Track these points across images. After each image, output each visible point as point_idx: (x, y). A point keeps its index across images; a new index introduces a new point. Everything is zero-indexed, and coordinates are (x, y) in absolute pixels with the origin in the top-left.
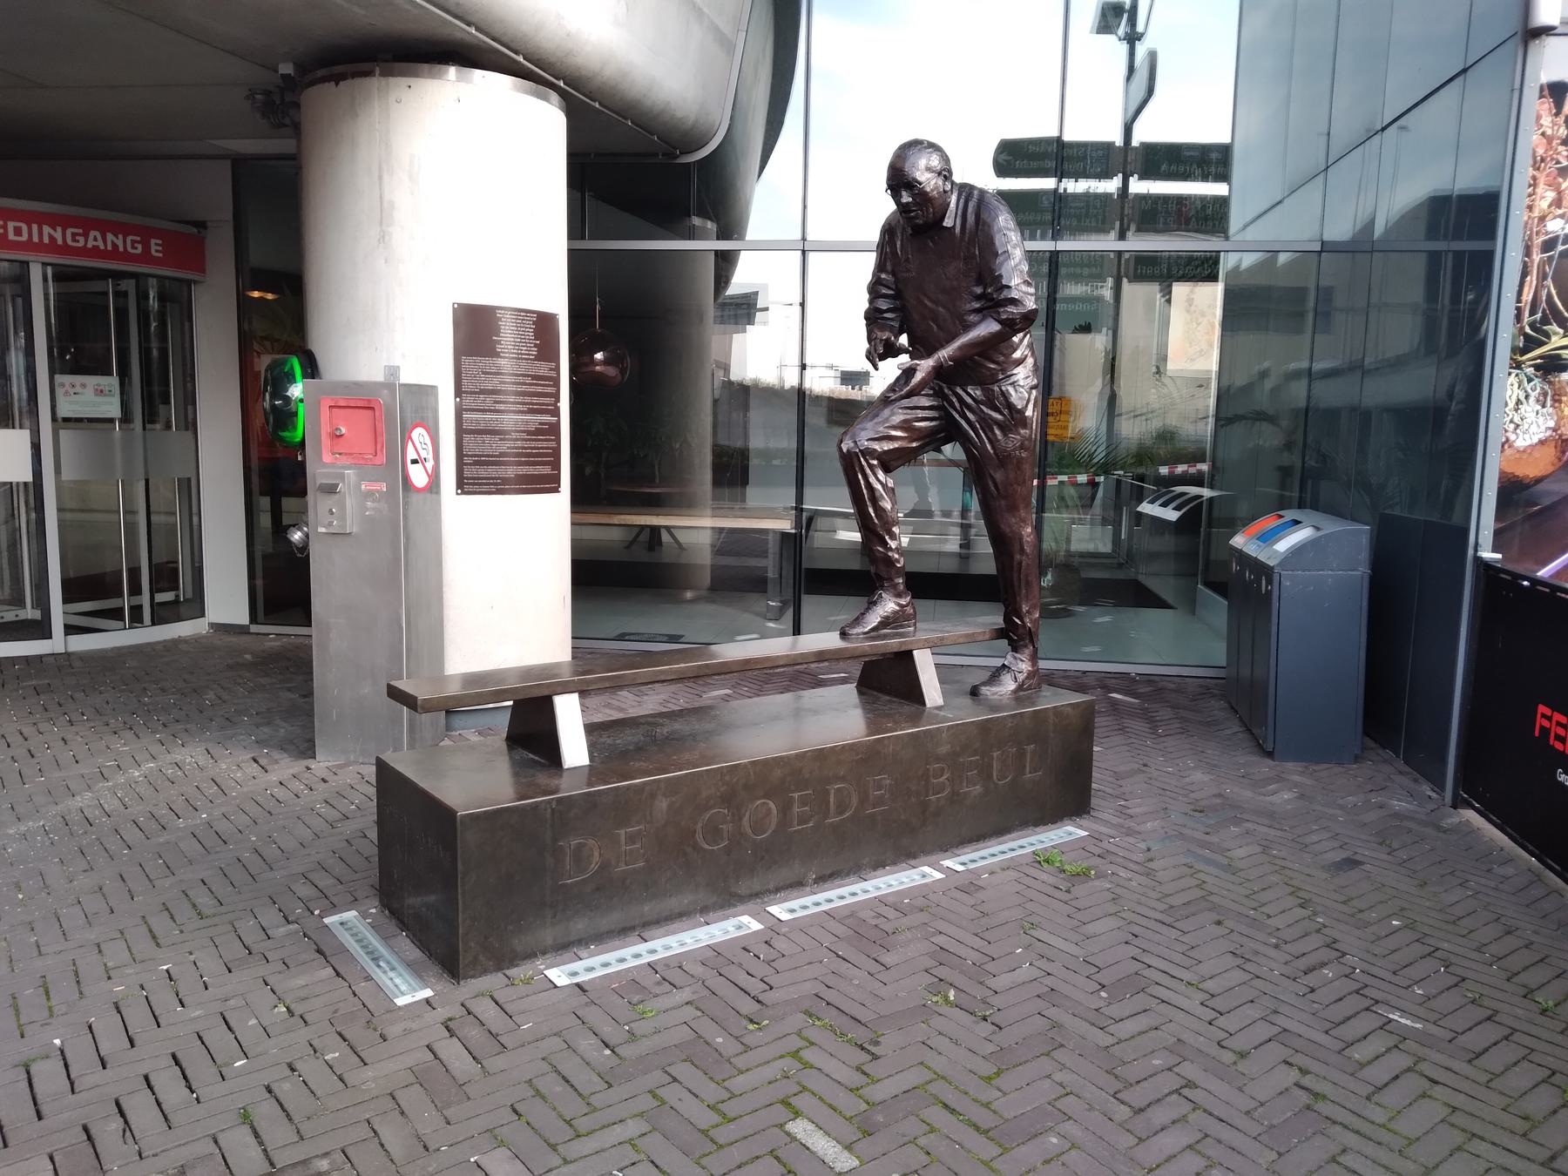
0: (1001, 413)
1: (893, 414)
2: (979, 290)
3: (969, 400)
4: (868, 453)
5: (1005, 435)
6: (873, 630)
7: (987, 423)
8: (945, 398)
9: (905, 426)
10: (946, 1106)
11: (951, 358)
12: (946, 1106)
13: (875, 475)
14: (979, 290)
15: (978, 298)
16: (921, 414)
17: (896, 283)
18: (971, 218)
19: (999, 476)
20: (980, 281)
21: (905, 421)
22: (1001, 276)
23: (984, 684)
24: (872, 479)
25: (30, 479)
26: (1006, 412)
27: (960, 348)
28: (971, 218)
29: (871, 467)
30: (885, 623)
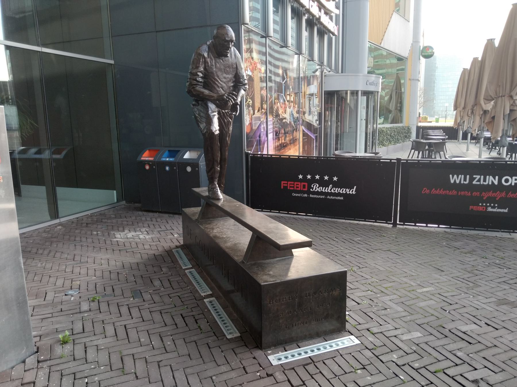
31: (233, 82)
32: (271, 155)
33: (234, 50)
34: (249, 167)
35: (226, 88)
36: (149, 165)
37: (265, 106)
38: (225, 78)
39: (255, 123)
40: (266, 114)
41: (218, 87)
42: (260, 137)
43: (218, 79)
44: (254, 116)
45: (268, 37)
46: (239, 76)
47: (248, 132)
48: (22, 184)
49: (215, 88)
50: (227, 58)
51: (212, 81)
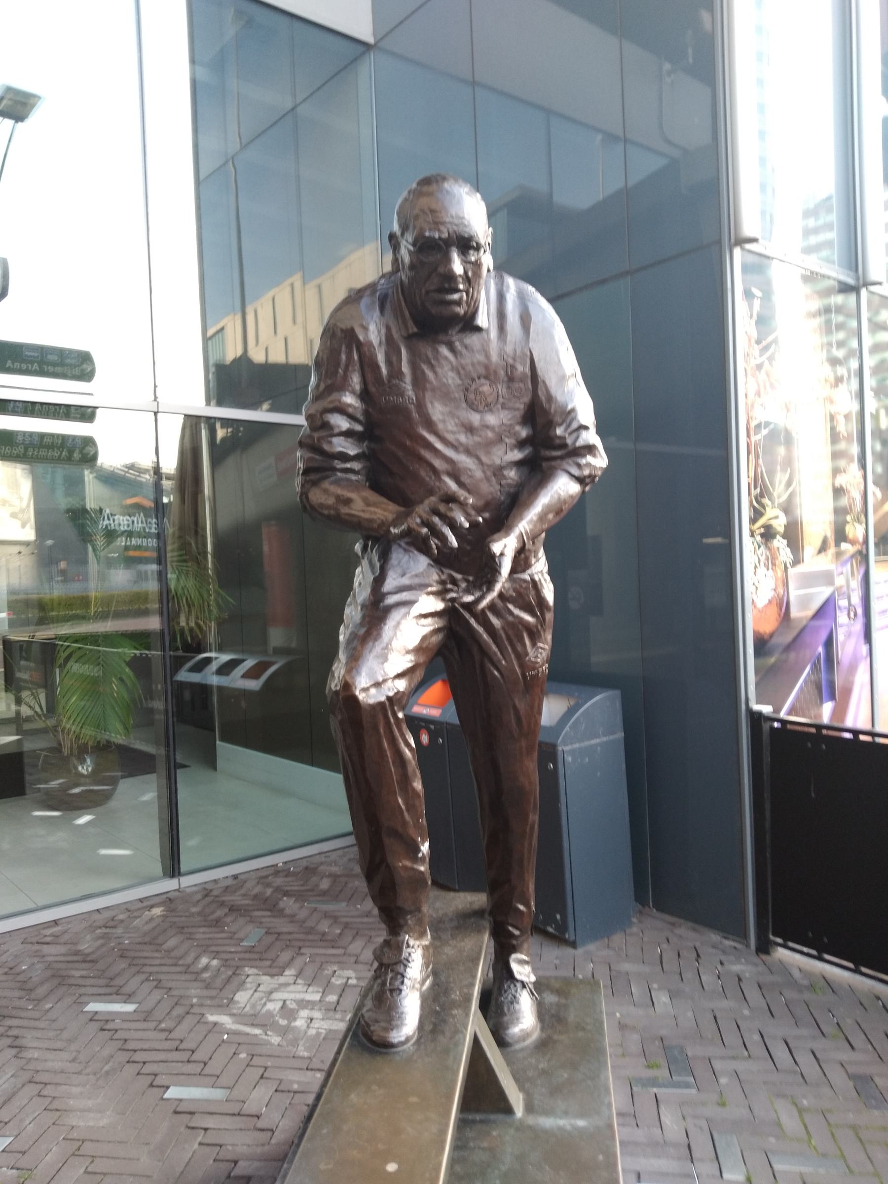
0: (533, 614)
17: (366, 413)
31: (521, 444)
32: (856, 733)
33: (522, 297)
34: (766, 769)
35: (479, 474)
36: (431, 734)
37: (855, 531)
38: (470, 429)
39: (805, 601)
40: (863, 557)
41: (435, 471)
42: (829, 643)
43: (432, 438)
44: (800, 569)
45: (866, 284)
46: (546, 412)
47: (767, 628)
48: (223, 739)
49: (416, 477)
50: (473, 340)
51: (402, 446)
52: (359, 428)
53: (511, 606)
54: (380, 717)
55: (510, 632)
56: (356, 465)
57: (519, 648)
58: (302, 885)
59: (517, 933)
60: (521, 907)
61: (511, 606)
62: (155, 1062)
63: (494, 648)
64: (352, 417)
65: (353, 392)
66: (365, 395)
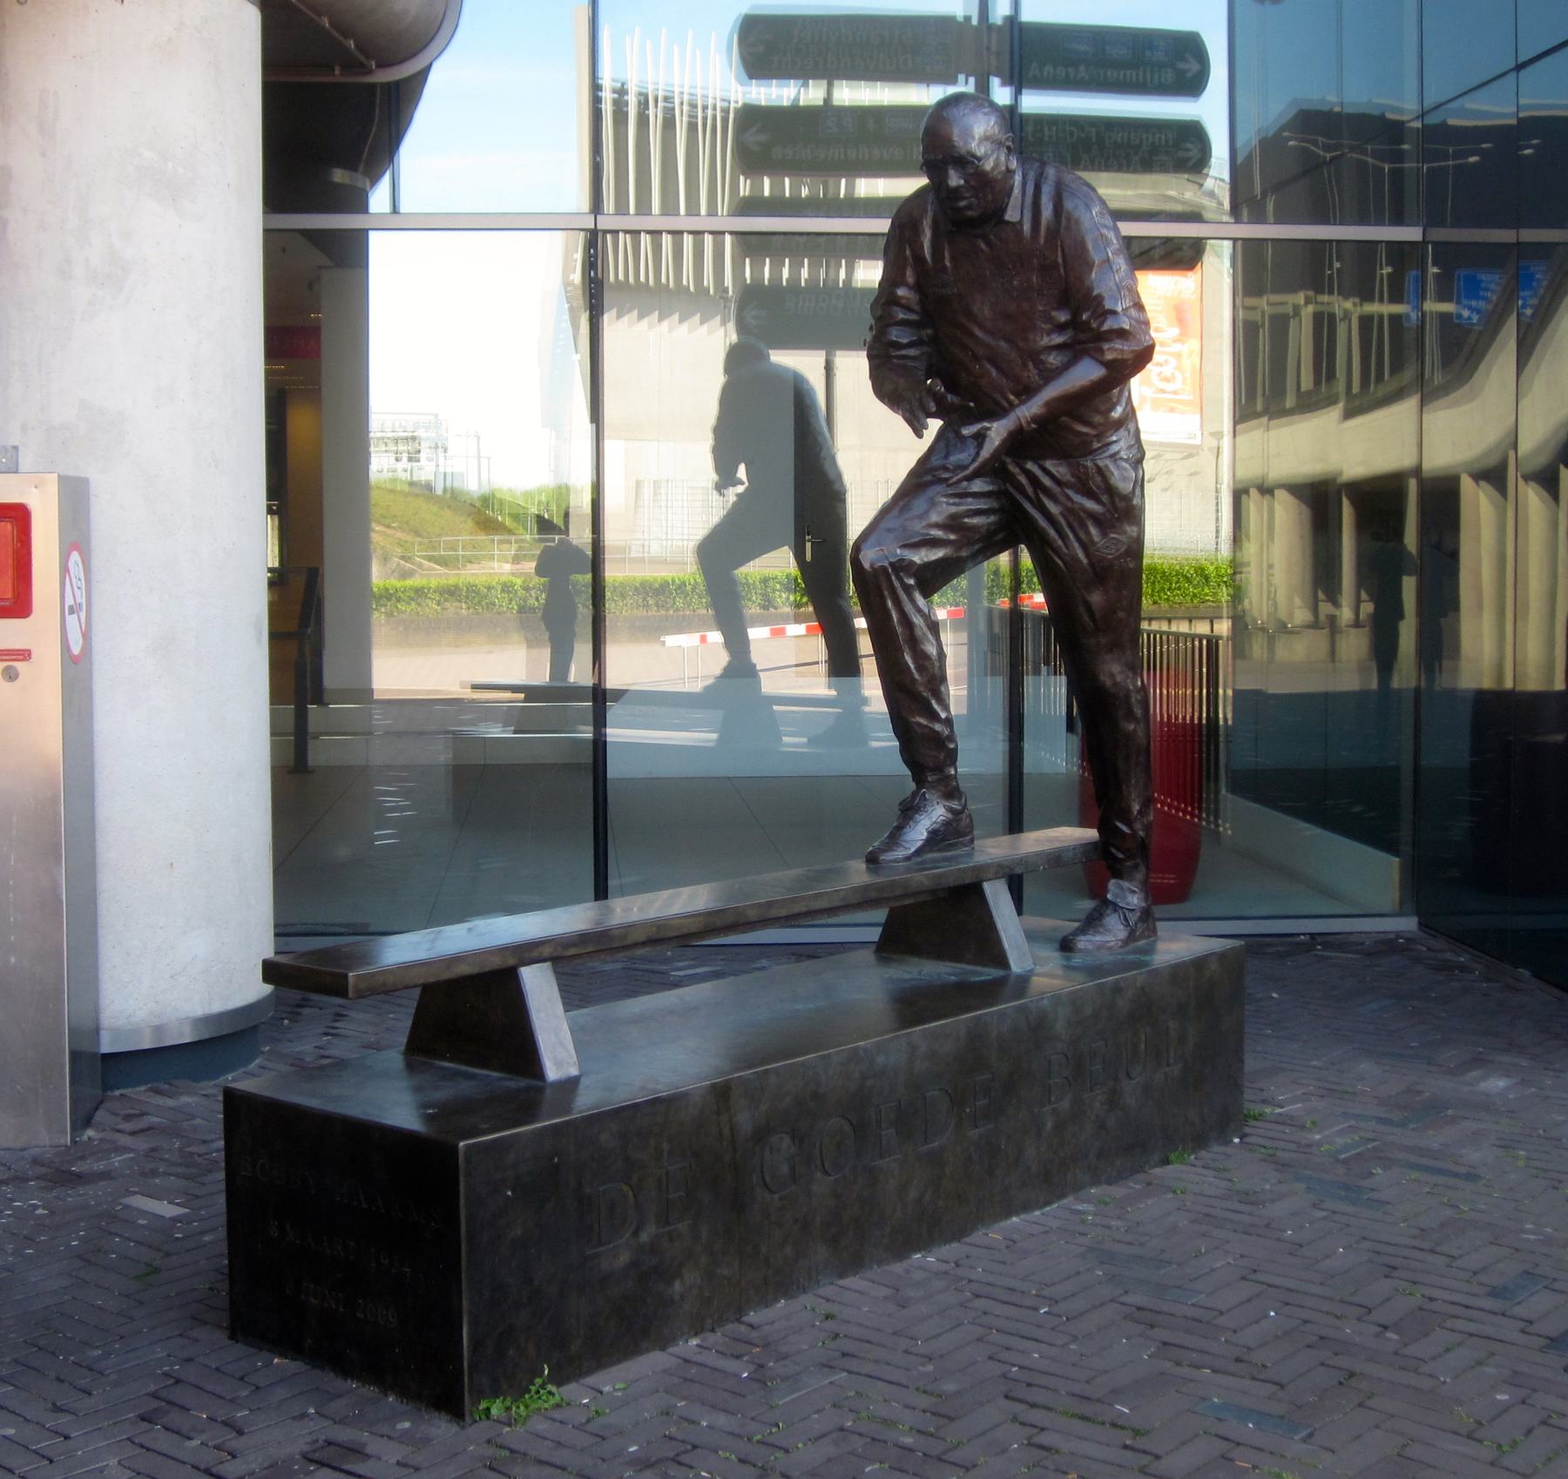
0: (1099, 501)
1: (933, 504)
2: (1063, 317)
3: (1047, 481)
4: (901, 567)
5: (1104, 534)
6: (918, 852)
7: (1077, 517)
8: (1010, 478)
9: (952, 524)
10: (1388, 1299)
11: (1035, 419)
12: (1388, 1299)
13: (913, 601)
14: (1063, 317)
15: (1061, 328)
16: (973, 504)
17: (922, 303)
18: (1047, 212)
19: (1096, 598)
20: (1064, 301)
21: (953, 517)
22: (1091, 289)
23: (1082, 931)
24: (908, 608)
25: (1029, 680)
26: (1105, 498)
27: (1048, 404)
28: (1047, 212)
29: (907, 589)
30: (936, 839)
52: (913, 317)
53: (1070, 493)
54: (883, 578)
55: (1071, 519)
56: (912, 352)
57: (1082, 536)
58: (1414, 1237)
59: (1121, 856)
60: (1125, 829)
61: (1070, 493)
62: (1026, 1402)
63: (1060, 542)
64: (907, 308)
65: (907, 285)
66: (918, 287)
